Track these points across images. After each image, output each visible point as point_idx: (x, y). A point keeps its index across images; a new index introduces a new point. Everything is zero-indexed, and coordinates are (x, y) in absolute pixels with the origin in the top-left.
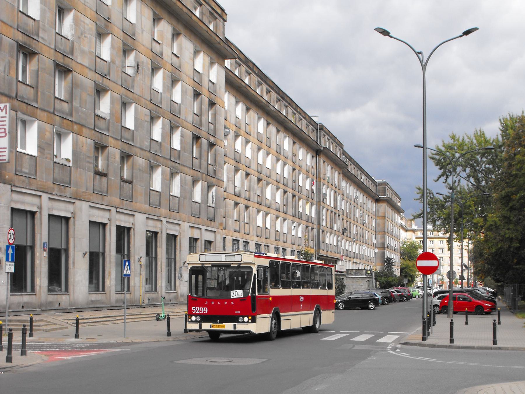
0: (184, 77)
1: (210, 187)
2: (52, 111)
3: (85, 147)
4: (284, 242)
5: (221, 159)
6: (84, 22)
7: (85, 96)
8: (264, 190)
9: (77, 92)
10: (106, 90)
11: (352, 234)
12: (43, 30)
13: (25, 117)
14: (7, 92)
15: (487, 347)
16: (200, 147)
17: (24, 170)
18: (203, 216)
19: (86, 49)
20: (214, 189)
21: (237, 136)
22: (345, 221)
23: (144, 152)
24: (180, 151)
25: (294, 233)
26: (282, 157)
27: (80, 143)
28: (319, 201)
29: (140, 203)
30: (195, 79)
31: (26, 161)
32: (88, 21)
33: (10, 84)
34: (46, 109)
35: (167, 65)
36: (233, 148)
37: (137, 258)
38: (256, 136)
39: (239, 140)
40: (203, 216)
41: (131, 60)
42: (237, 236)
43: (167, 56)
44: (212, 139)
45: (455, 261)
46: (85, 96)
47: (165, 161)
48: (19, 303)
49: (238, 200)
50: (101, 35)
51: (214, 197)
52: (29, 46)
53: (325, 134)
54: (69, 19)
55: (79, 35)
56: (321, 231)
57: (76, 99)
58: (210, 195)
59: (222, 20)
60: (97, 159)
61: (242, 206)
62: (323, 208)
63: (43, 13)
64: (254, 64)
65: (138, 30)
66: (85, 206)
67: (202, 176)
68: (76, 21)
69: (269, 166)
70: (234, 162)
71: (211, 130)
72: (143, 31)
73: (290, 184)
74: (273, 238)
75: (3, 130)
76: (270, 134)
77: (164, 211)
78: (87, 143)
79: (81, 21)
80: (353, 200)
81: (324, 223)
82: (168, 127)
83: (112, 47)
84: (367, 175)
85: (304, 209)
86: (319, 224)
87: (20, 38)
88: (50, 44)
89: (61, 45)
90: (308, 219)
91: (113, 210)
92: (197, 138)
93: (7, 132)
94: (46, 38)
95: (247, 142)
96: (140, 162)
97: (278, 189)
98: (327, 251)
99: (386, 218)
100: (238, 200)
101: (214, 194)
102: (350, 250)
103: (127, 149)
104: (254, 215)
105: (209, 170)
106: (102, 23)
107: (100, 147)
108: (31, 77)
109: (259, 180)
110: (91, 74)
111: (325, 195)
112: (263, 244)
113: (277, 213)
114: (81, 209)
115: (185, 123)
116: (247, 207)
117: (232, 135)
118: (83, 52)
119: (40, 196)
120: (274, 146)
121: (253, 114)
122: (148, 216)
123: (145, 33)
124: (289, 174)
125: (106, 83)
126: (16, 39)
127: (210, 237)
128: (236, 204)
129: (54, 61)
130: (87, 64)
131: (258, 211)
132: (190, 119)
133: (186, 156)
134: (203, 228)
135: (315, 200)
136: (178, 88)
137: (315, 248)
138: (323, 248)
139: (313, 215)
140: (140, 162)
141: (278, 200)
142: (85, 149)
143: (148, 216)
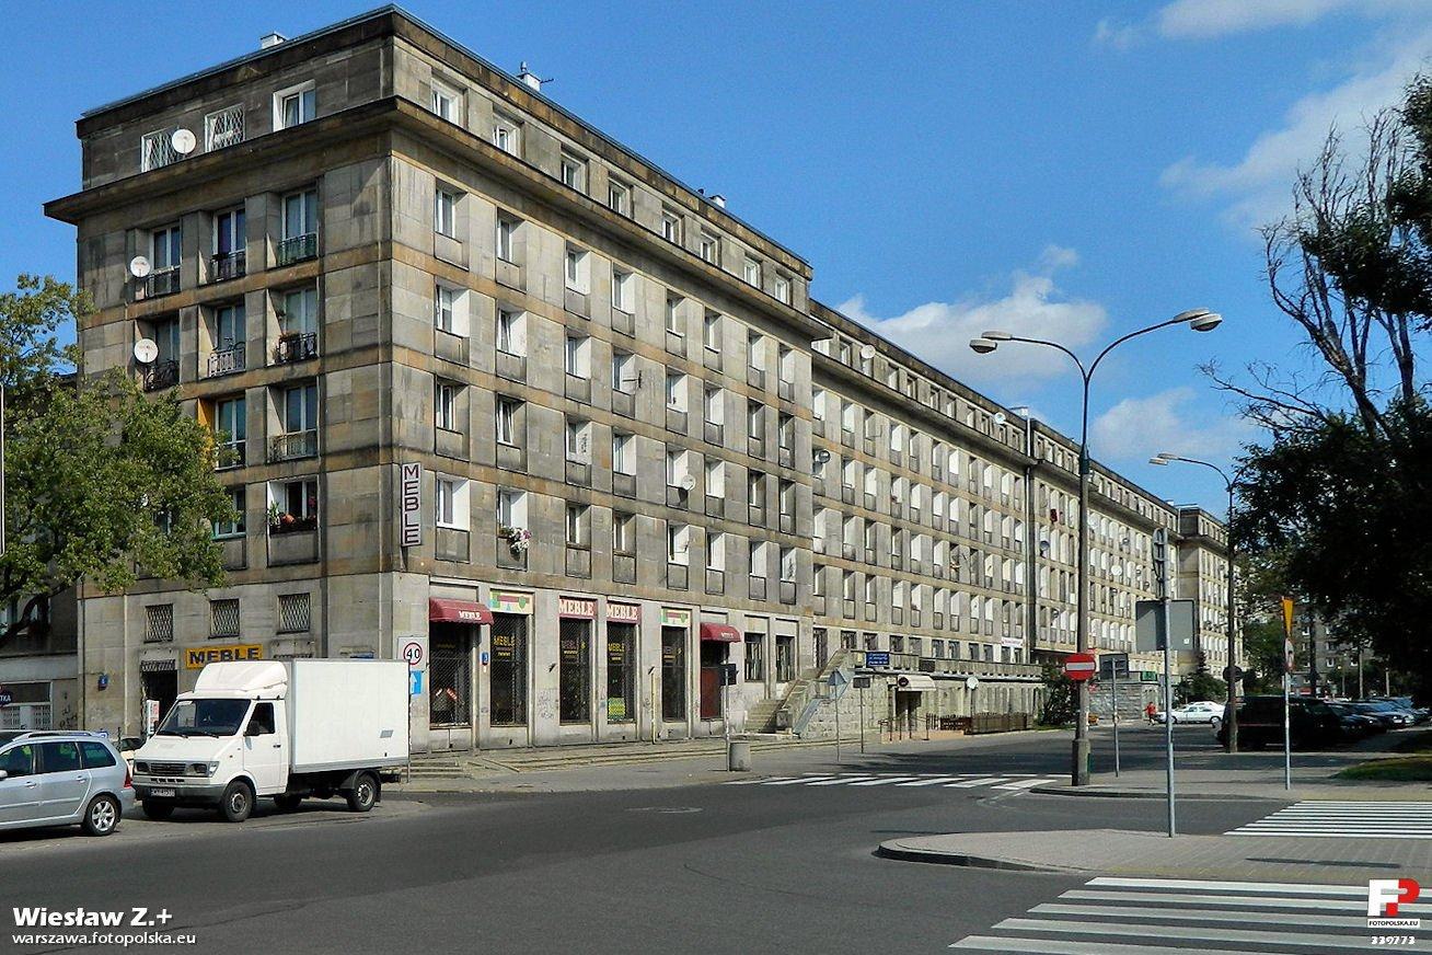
0: (728, 381)
1: (784, 551)
2: (493, 463)
3: (549, 510)
4: (952, 629)
5: (806, 505)
6: (544, 328)
7: (548, 436)
8: (906, 545)
9: (532, 431)
10: (584, 422)
11: (1116, 608)
12: (476, 349)
13: (451, 478)
14: (420, 447)
15: (1392, 783)
16: (763, 488)
17: (449, 552)
18: (773, 597)
19: (549, 365)
20: (792, 554)
21: (845, 461)
22: (1098, 586)
23: (655, 507)
24: (723, 499)
25: (975, 613)
26: (944, 485)
27: (541, 508)
28: (1033, 555)
29: (650, 581)
30: (752, 382)
31: (453, 538)
32: (549, 324)
33: (425, 434)
34: (482, 462)
35: (696, 367)
36: (839, 482)
37: (645, 669)
38: (886, 457)
39: (850, 467)
40: (773, 597)
41: (628, 369)
42: (849, 625)
43: (695, 350)
44: (787, 475)
45: (333, 547)
46: (548, 436)
47: (695, 516)
48: (444, 741)
49: (851, 566)
50: (574, 339)
51: (794, 567)
52: (454, 376)
53: (1043, 436)
54: (519, 326)
55: (536, 347)
56: (1038, 607)
57: (532, 442)
58: (786, 561)
59: (803, 279)
60: (572, 524)
61: (860, 576)
62: (1042, 566)
63: (474, 324)
64: (879, 338)
65: (639, 323)
66: (551, 596)
67: (769, 535)
68: (530, 329)
69: (916, 503)
70: (841, 504)
71: (786, 459)
72: (648, 322)
73: (965, 530)
74: (928, 622)
75: (414, 501)
76: (917, 448)
77: (693, 594)
78: (553, 503)
79: (539, 326)
80: (1117, 546)
81: (1044, 594)
82: (700, 463)
83: (594, 355)
84: (1153, 499)
85: (998, 571)
86: (1033, 594)
87: (440, 366)
88: (487, 368)
89: (507, 367)
90: (1008, 587)
91: (602, 600)
92: (755, 475)
93: (419, 502)
94: (480, 361)
95: (867, 469)
96: (649, 522)
97: (936, 541)
98: (1053, 642)
99: (1201, 574)
100: (851, 566)
101: (794, 561)
102: (1112, 637)
103: (623, 504)
104: (887, 589)
105: (67, 676)
106: (576, 323)
107: (575, 507)
108: (459, 421)
109: (896, 530)
110: (558, 402)
111: (1045, 544)
112: (906, 637)
113: (935, 582)
114: (545, 602)
115: (732, 453)
116: (870, 577)
117: (835, 458)
118: (543, 372)
119: (476, 587)
120: (926, 470)
121: (882, 418)
122: (664, 604)
123: (652, 327)
124: (961, 513)
125: (584, 410)
126: (433, 370)
127: (787, 630)
128: (847, 573)
129: (496, 392)
130: (550, 389)
131: (895, 582)
132: (743, 446)
133: (736, 509)
134: (773, 616)
135: (1024, 552)
136: (717, 400)
137: (1025, 637)
138: (1043, 637)
139: (1020, 579)
140: (649, 522)
141: (938, 560)
142: (550, 513)
143: (664, 604)
